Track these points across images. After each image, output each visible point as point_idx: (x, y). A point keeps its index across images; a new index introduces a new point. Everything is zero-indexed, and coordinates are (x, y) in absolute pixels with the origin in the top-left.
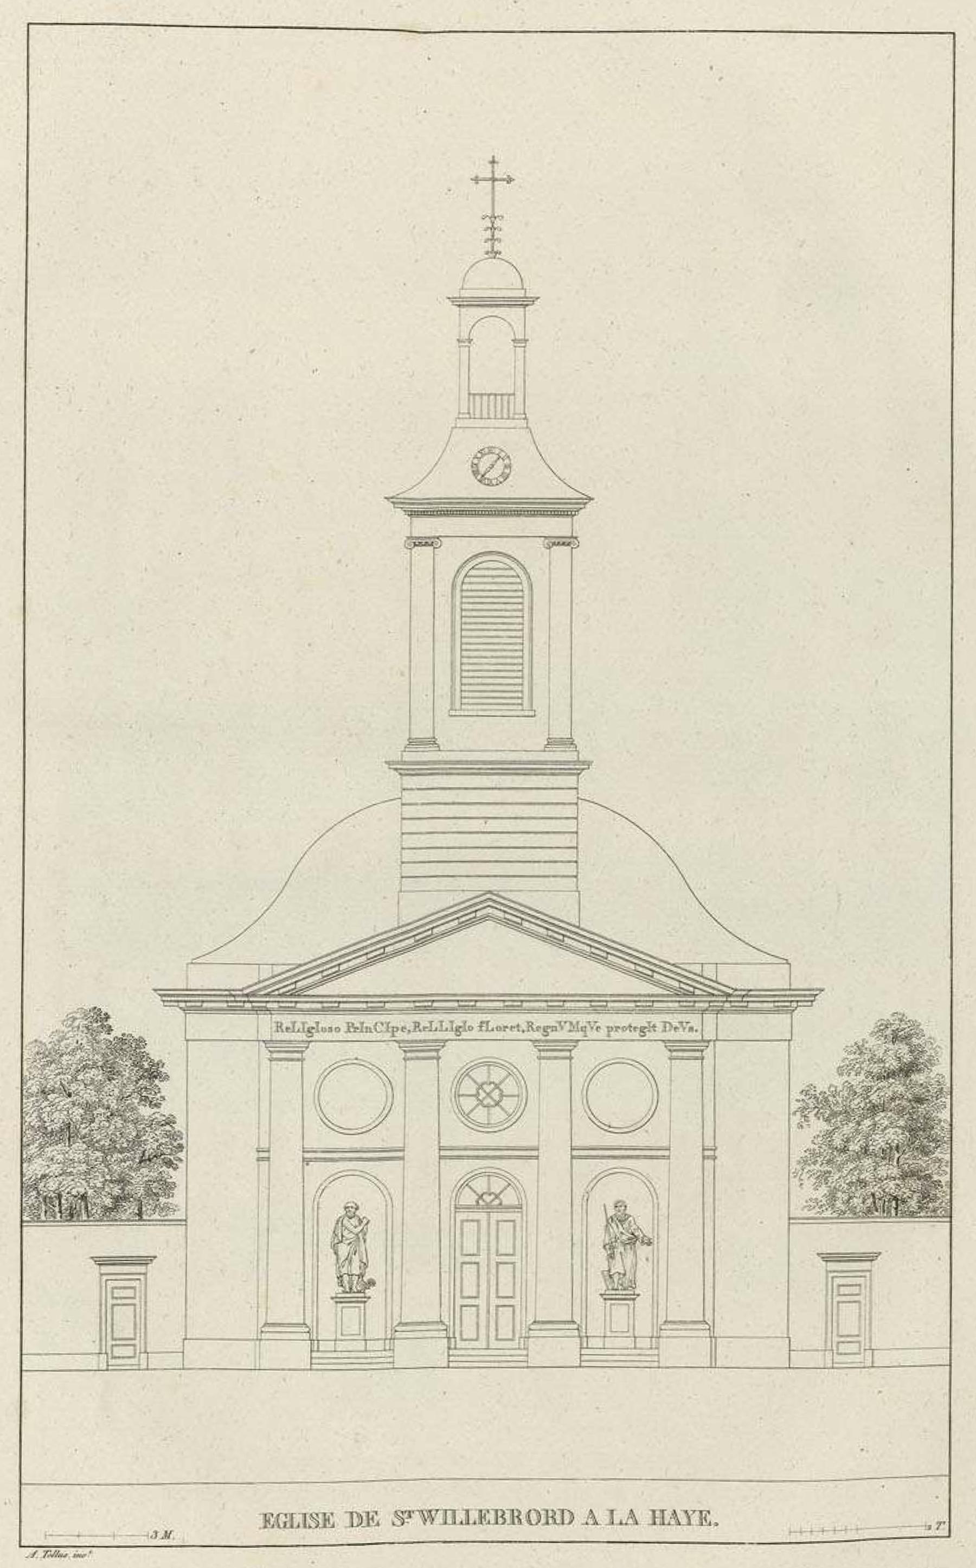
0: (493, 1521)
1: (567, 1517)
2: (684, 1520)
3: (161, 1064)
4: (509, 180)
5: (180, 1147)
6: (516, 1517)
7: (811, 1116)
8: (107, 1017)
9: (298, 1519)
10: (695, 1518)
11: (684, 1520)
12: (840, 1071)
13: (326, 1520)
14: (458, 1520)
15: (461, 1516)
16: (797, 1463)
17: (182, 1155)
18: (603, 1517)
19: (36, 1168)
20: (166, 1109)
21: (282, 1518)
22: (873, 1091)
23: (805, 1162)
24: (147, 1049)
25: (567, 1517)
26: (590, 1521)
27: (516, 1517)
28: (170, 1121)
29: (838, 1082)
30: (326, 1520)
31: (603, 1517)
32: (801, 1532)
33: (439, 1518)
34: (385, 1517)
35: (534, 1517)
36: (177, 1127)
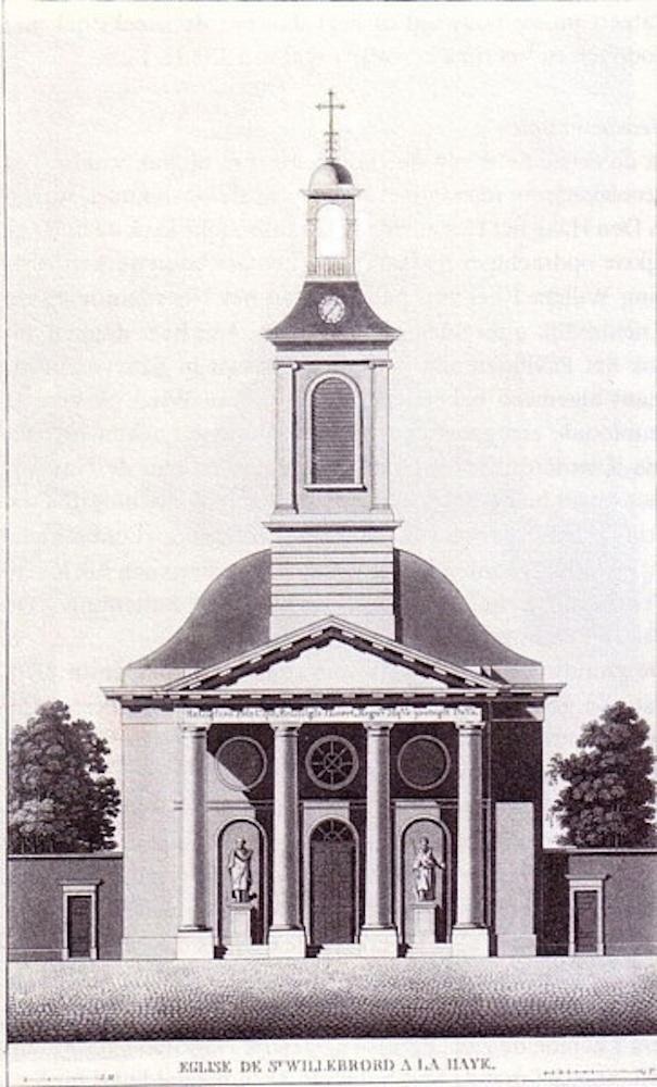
0: (337, 1068)
1: (389, 1065)
2: (470, 1065)
3: (105, 741)
4: (342, 107)
5: (119, 802)
6: (354, 1066)
7: (559, 777)
8: (67, 708)
9: (205, 1066)
10: (479, 1064)
11: (470, 1065)
12: (580, 744)
13: (225, 1066)
14: (313, 1068)
15: (315, 1065)
16: (541, 985)
17: (119, 807)
18: (414, 1064)
19: (18, 817)
20: (108, 775)
21: (194, 1065)
22: (97, 854)
23: (555, 809)
24: (94, 731)
25: (389, 1065)
26: (406, 1067)
27: (354, 1066)
28: (111, 782)
29: (578, 752)
30: (225, 1066)
31: (414, 1064)
32: (331, 133)
33: (300, 1066)
34: (264, 1065)
35: (366, 1065)
36: (116, 787)
